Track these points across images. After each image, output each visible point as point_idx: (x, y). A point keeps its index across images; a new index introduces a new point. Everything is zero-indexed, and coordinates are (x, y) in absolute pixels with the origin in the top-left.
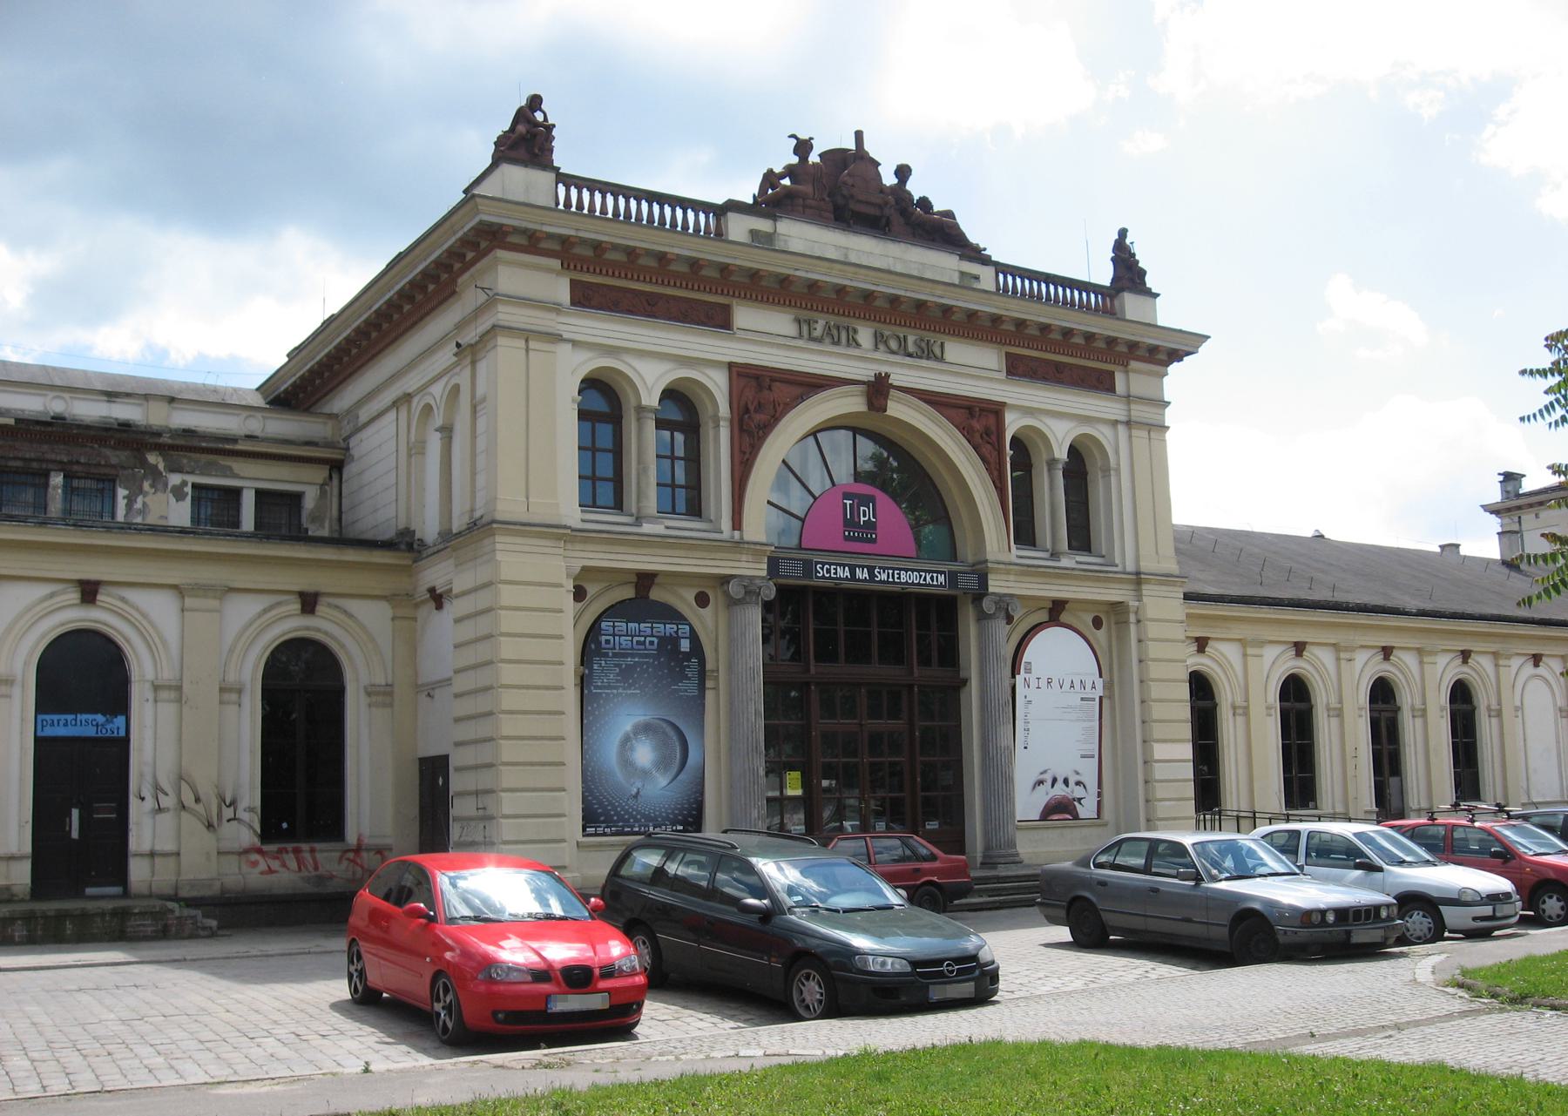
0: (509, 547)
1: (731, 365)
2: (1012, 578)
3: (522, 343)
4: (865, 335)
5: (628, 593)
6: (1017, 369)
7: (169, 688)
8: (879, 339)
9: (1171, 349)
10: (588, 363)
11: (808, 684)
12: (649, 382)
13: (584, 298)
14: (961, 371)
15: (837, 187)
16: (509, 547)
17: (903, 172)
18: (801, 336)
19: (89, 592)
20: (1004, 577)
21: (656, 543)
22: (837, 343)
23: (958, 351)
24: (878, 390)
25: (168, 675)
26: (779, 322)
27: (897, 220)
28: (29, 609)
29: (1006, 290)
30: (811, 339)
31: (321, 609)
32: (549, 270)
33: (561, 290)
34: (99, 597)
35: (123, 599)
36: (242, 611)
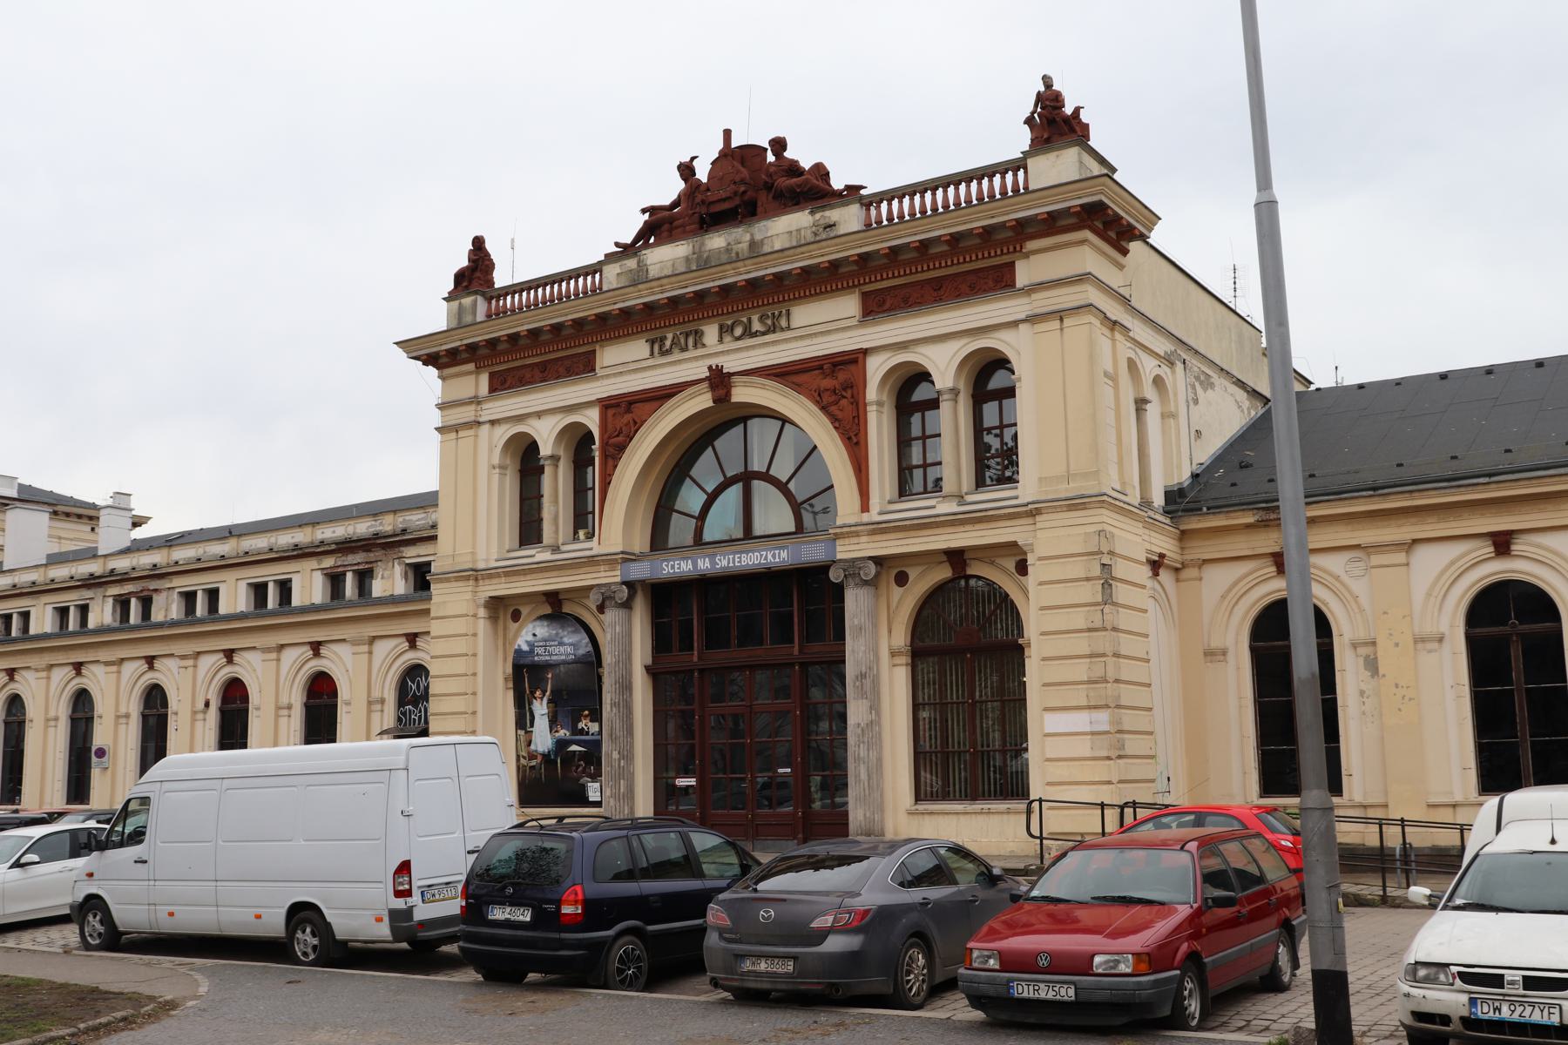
0: (1048, 524)
1: (600, 400)
2: (864, 539)
3: (1057, 324)
4: (711, 332)
5: (944, 573)
6: (876, 307)
7: (1366, 644)
8: (724, 330)
9: (437, 354)
10: (504, 433)
11: (692, 671)
12: (546, 434)
13: (500, 384)
14: (623, 370)
15: (751, 182)
16: (1048, 524)
17: (779, 145)
18: (652, 354)
19: (1502, 543)
20: (855, 540)
21: (561, 562)
22: (684, 349)
23: (806, 314)
24: (719, 381)
25: (1362, 634)
26: (637, 349)
27: (763, 198)
28: (1453, 563)
29: (992, 196)
30: (663, 353)
31: (1516, 548)
32: (470, 373)
33: (847, 306)
34: (1513, 547)
35: (1539, 546)
36: (1431, 562)
